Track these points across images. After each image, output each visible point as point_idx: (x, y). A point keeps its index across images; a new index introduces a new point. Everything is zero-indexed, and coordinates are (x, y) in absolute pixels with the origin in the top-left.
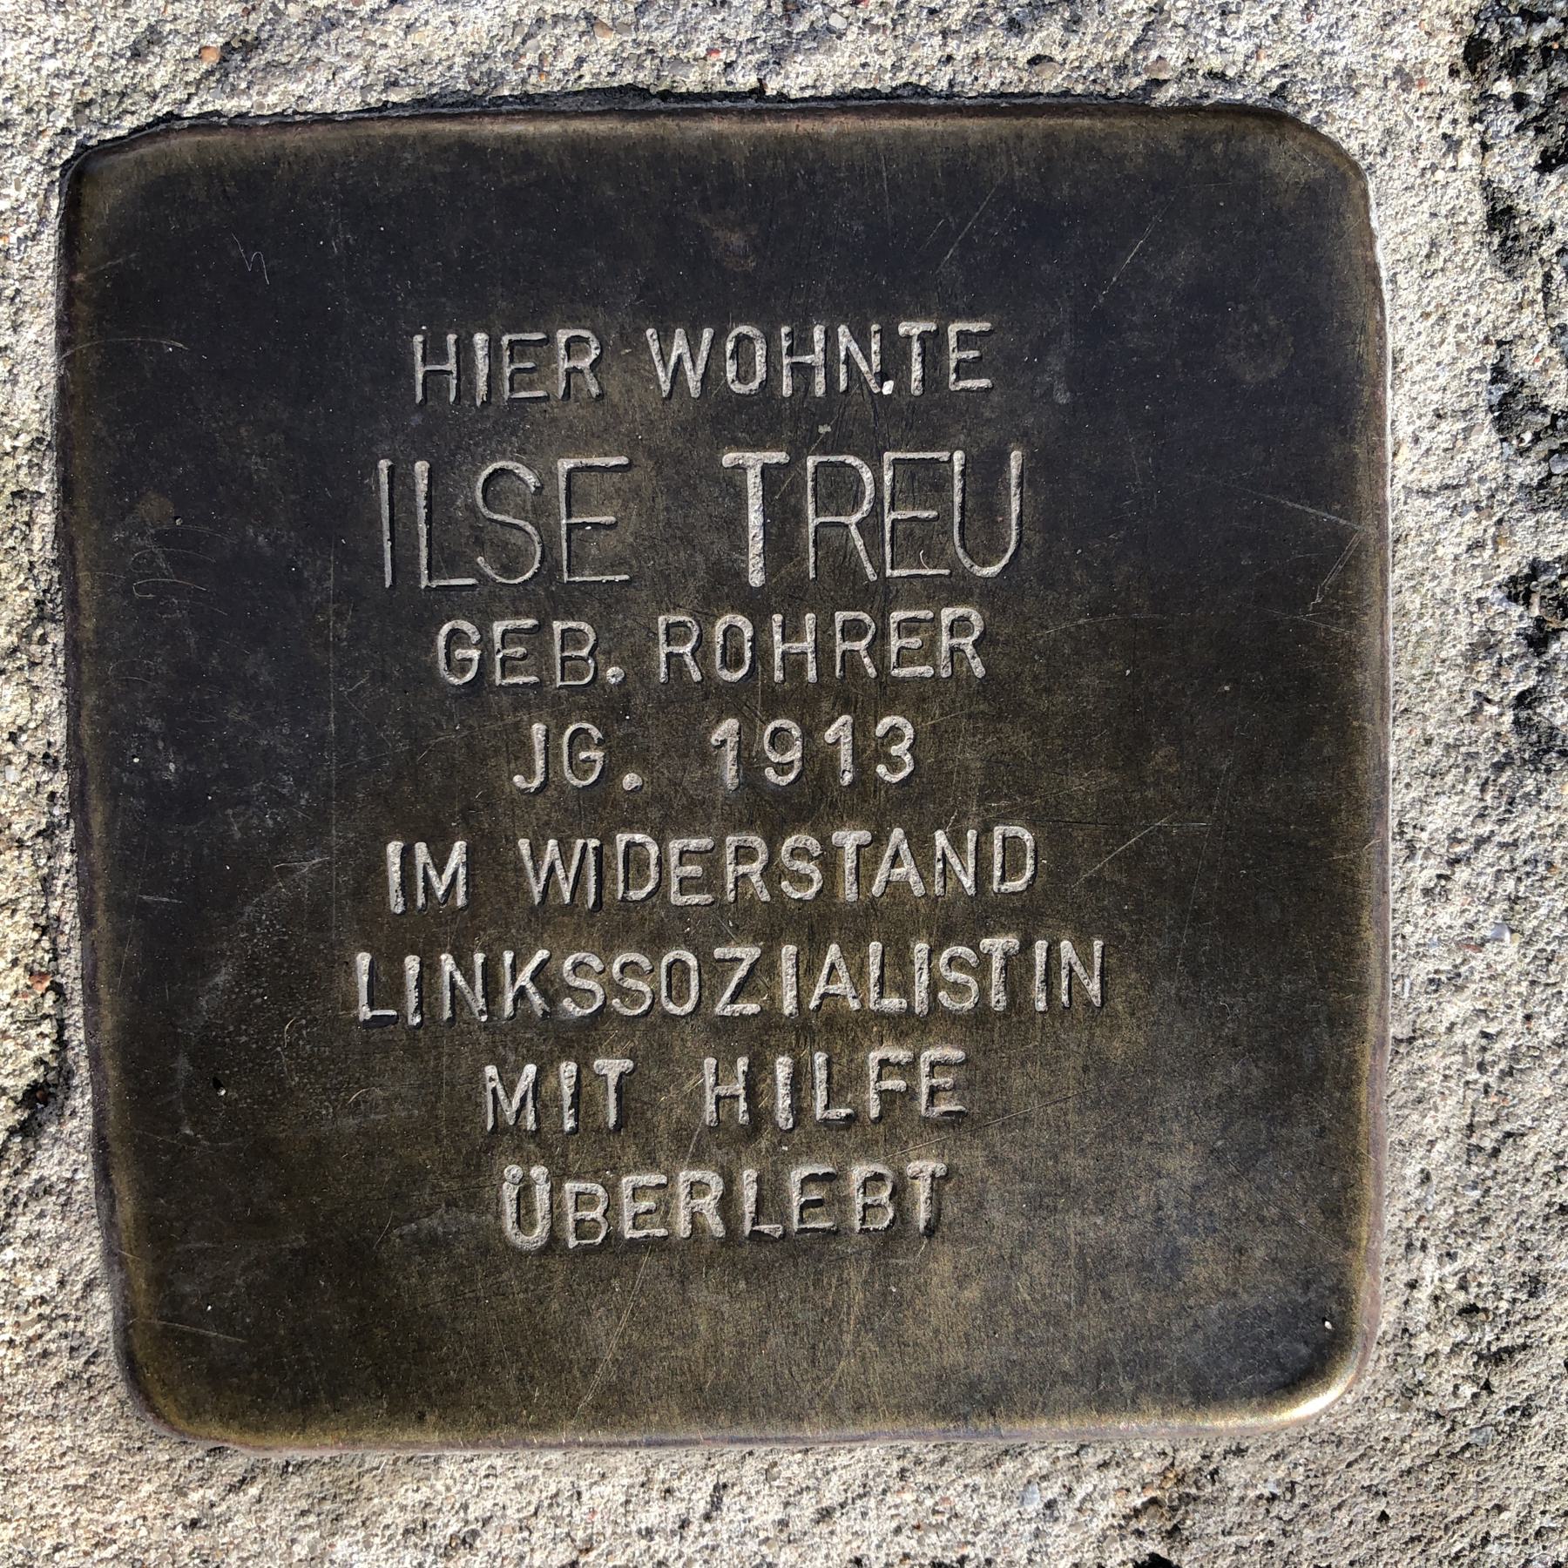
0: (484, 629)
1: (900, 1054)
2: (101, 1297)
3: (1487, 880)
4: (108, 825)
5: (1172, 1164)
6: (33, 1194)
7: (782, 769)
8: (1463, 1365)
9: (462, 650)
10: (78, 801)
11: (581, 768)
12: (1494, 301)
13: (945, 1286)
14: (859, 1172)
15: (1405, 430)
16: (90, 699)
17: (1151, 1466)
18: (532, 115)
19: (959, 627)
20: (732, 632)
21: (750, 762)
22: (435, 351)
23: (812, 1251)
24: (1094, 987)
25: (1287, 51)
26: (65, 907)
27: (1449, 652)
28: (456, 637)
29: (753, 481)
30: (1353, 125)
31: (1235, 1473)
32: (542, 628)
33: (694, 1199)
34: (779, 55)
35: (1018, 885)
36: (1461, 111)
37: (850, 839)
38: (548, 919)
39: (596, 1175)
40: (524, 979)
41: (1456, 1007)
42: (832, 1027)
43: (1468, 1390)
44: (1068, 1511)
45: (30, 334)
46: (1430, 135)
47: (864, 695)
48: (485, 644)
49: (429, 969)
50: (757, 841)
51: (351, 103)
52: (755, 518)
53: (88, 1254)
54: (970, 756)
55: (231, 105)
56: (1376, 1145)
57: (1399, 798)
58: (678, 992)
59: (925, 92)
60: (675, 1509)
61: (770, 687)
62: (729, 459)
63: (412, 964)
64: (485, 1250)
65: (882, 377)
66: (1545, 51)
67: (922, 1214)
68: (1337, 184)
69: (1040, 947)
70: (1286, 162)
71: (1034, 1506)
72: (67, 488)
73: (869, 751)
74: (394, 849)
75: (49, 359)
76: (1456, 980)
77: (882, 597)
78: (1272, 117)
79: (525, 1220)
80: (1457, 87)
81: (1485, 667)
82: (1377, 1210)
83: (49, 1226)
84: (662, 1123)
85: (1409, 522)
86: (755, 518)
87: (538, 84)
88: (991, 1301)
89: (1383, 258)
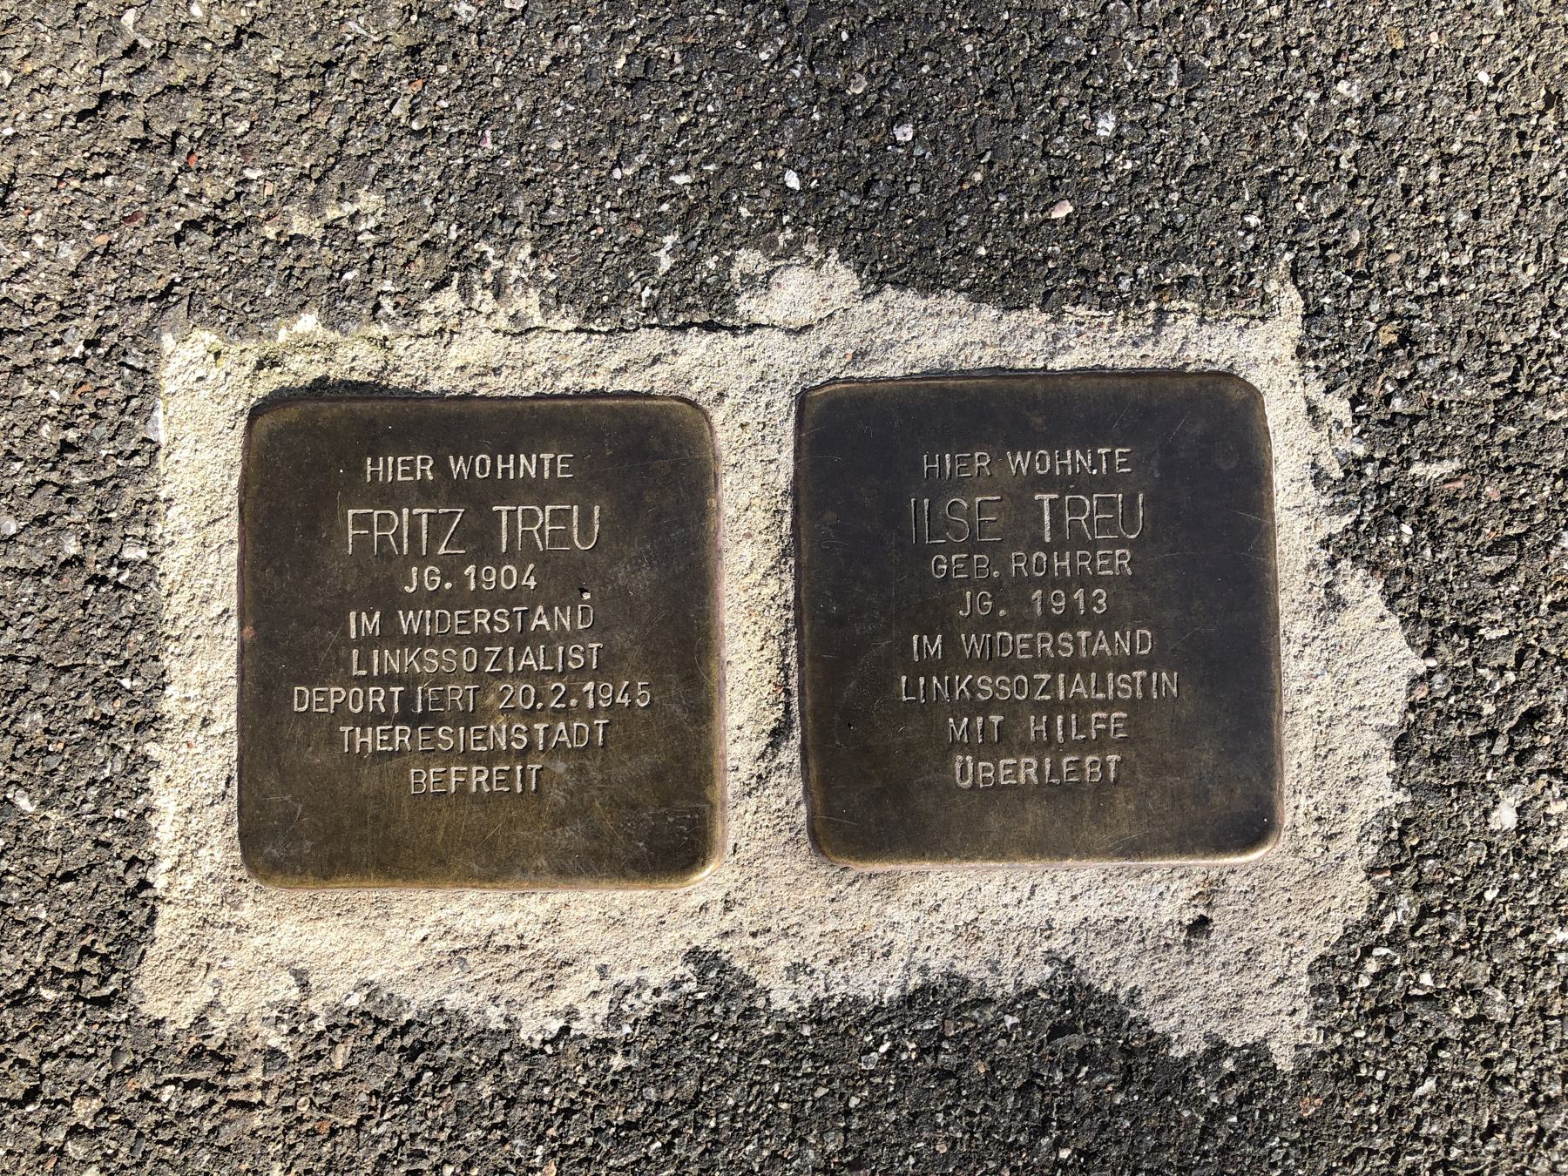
0: (949, 558)
1: (1103, 715)
2: (803, 808)
3: (1317, 652)
4: (811, 629)
5: (1204, 757)
6: (777, 769)
7: (1058, 608)
8: (1317, 840)
9: (941, 565)
10: (798, 621)
11: (983, 608)
12: (1311, 439)
13: (1123, 804)
14: (1089, 759)
15: (1280, 487)
16: (804, 584)
17: (1200, 878)
18: (964, 378)
19: (1122, 557)
20: (1039, 558)
21: (1046, 606)
22: (931, 460)
23: (1070, 791)
24: (1175, 690)
25: (1233, 352)
26: (792, 660)
27: (1299, 568)
28: (938, 561)
29: (1046, 504)
30: (1257, 378)
31: (1232, 881)
32: (970, 557)
33: (1027, 769)
34: (1052, 355)
35: (1145, 652)
36: (1296, 372)
37: (1083, 634)
38: (973, 665)
39: (991, 760)
40: (963, 686)
41: (1308, 700)
42: (1080, 706)
43: (1320, 850)
44: (1168, 896)
45: (784, 454)
46: (1286, 381)
47: (1088, 581)
48: (949, 563)
49: (928, 681)
50: (1049, 635)
51: (900, 373)
52: (1047, 518)
53: (797, 791)
54: (1127, 604)
55: (857, 375)
56: (1281, 752)
57: (1283, 621)
58: (1020, 691)
59: (1104, 368)
60: (1017, 895)
61: (1054, 578)
62: (1037, 497)
63: (922, 680)
64: (949, 788)
65: (1092, 468)
66: (1325, 351)
67: (1112, 775)
68: (1253, 398)
69: (1155, 675)
70: (1236, 394)
71: (1155, 894)
72: (796, 509)
73: (1090, 602)
74: (915, 638)
75: (791, 463)
76: (1308, 690)
77: (1094, 546)
78: (1228, 376)
79: (964, 776)
80: (1294, 363)
81: (1313, 573)
82: (1282, 776)
83: (783, 781)
84: (1014, 740)
85: (1283, 520)
86: (1047, 518)
87: (965, 366)
88: (1138, 809)
89: (1270, 425)
